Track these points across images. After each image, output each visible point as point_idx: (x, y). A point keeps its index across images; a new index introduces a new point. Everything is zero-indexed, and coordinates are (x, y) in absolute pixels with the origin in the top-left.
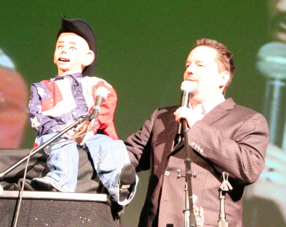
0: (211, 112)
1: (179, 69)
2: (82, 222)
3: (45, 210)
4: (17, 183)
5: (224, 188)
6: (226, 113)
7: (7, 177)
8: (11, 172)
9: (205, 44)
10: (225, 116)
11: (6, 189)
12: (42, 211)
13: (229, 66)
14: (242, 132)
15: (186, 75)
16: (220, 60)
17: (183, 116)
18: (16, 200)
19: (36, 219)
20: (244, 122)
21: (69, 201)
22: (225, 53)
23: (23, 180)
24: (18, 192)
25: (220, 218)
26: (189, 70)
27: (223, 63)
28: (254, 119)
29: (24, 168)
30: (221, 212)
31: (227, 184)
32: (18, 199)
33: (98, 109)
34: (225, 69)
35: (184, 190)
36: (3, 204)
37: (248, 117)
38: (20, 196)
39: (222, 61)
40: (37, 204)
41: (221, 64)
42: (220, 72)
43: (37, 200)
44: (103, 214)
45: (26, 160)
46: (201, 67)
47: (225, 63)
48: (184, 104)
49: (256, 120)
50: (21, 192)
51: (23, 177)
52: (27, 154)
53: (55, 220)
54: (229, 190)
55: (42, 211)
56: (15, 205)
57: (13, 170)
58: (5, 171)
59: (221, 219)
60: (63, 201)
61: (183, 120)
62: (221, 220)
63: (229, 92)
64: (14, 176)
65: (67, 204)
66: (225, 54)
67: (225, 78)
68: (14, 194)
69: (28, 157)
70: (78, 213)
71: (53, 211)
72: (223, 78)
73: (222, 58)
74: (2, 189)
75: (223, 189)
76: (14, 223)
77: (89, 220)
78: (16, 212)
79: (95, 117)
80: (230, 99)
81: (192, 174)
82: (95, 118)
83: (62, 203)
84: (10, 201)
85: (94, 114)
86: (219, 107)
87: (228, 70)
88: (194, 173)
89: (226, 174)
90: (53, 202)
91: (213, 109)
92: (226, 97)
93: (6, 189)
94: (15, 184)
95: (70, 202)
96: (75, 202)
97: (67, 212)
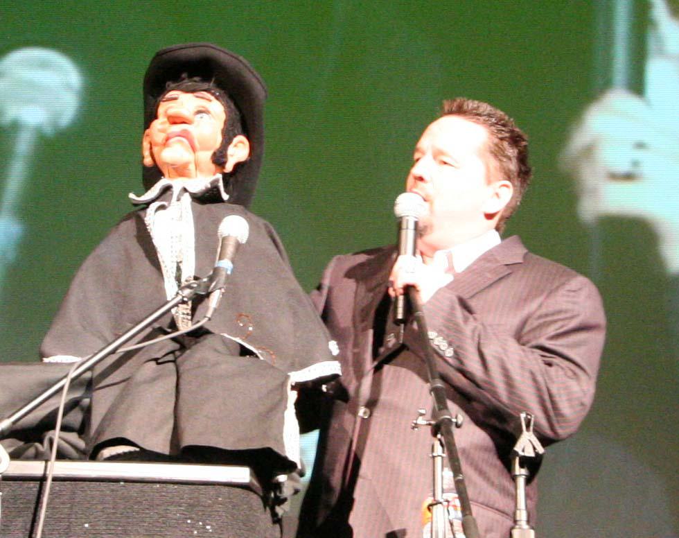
0: (470, 270)
1: (396, 169)
2: (192, 532)
3: (107, 506)
4: (41, 442)
5: (523, 451)
6: (507, 273)
7: (19, 428)
8: (26, 417)
9: (460, 111)
10: (501, 279)
11: (15, 456)
12: (100, 507)
13: (513, 166)
14: (541, 321)
15: (410, 181)
16: (492, 152)
17: (410, 281)
18: (39, 482)
19: (87, 525)
20: (548, 296)
21: (162, 485)
22: (506, 137)
23: (54, 435)
24: (43, 463)
25: (515, 522)
26: (417, 170)
27: (501, 160)
28: (569, 291)
29: (57, 406)
30: (519, 507)
31: (530, 441)
32: (43, 479)
33: (226, 267)
34: (501, 175)
35: (431, 455)
36: (8, 492)
37: (556, 284)
38: (48, 472)
39: (496, 156)
40: (89, 492)
41: (493, 163)
42: (489, 182)
43: (88, 483)
44: (242, 513)
45: (61, 389)
46: (446, 166)
47: (505, 160)
48: (405, 249)
49: (574, 291)
50: (49, 463)
51: (53, 428)
52: (64, 375)
53: (130, 528)
54: (537, 454)
55: (100, 507)
56: (36, 493)
57: (30, 414)
58: (13, 414)
59: (519, 523)
60: (149, 485)
61: (409, 290)
62: (517, 527)
63: (509, 225)
64: (34, 425)
65: (158, 491)
66: (507, 139)
67: (503, 196)
68: (34, 468)
69: (66, 382)
70: (183, 510)
71: (125, 508)
72: (497, 195)
73: (497, 149)
74: (7, 457)
75: (521, 453)
76: (42, 491)
77: (208, 527)
78: (39, 508)
79: (220, 286)
80: (514, 238)
81: (454, 420)
82: (220, 289)
83: (147, 487)
84: (26, 484)
85: (217, 279)
86: (487, 257)
87: (509, 178)
88: (456, 418)
89: (529, 417)
90: (124, 486)
91: (474, 264)
92: (503, 237)
93: (15, 456)
94: (38, 445)
95: (164, 485)
96: (176, 487)
97: (157, 509)
